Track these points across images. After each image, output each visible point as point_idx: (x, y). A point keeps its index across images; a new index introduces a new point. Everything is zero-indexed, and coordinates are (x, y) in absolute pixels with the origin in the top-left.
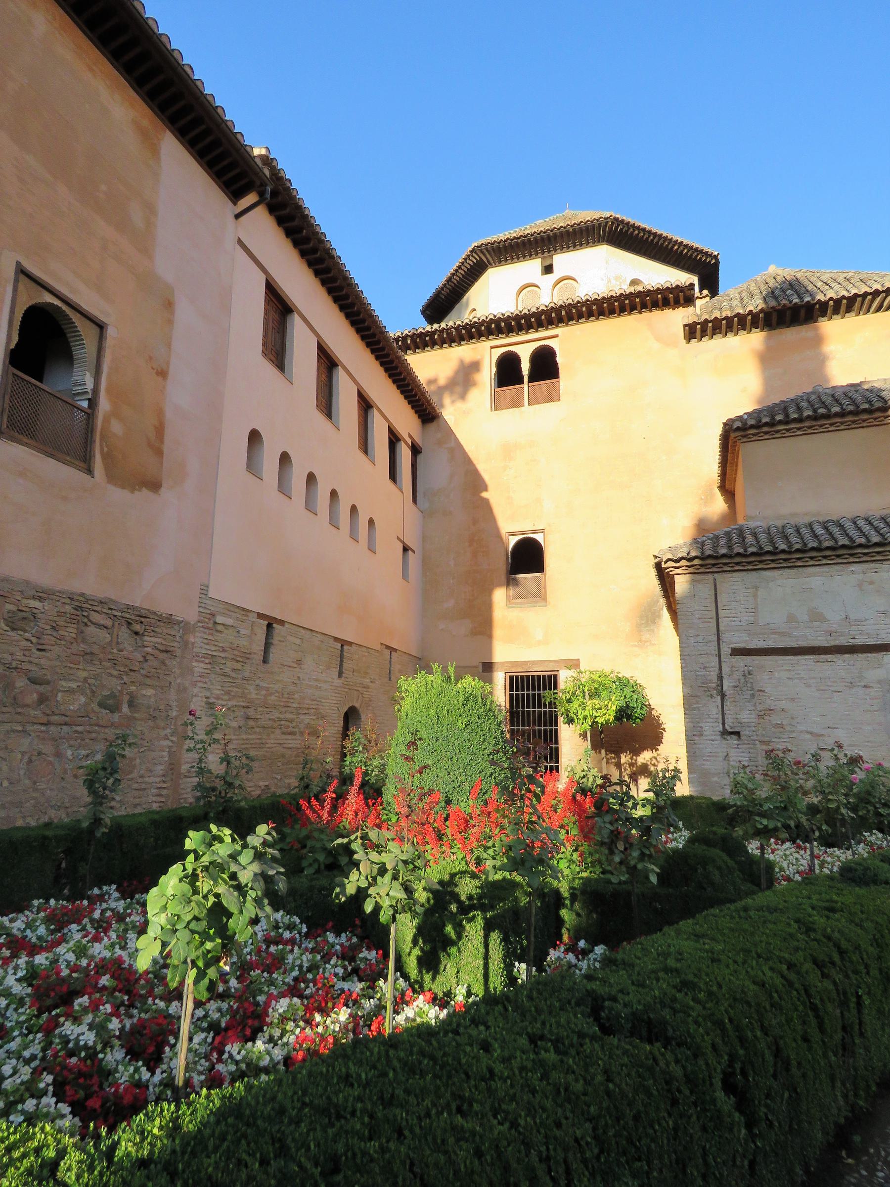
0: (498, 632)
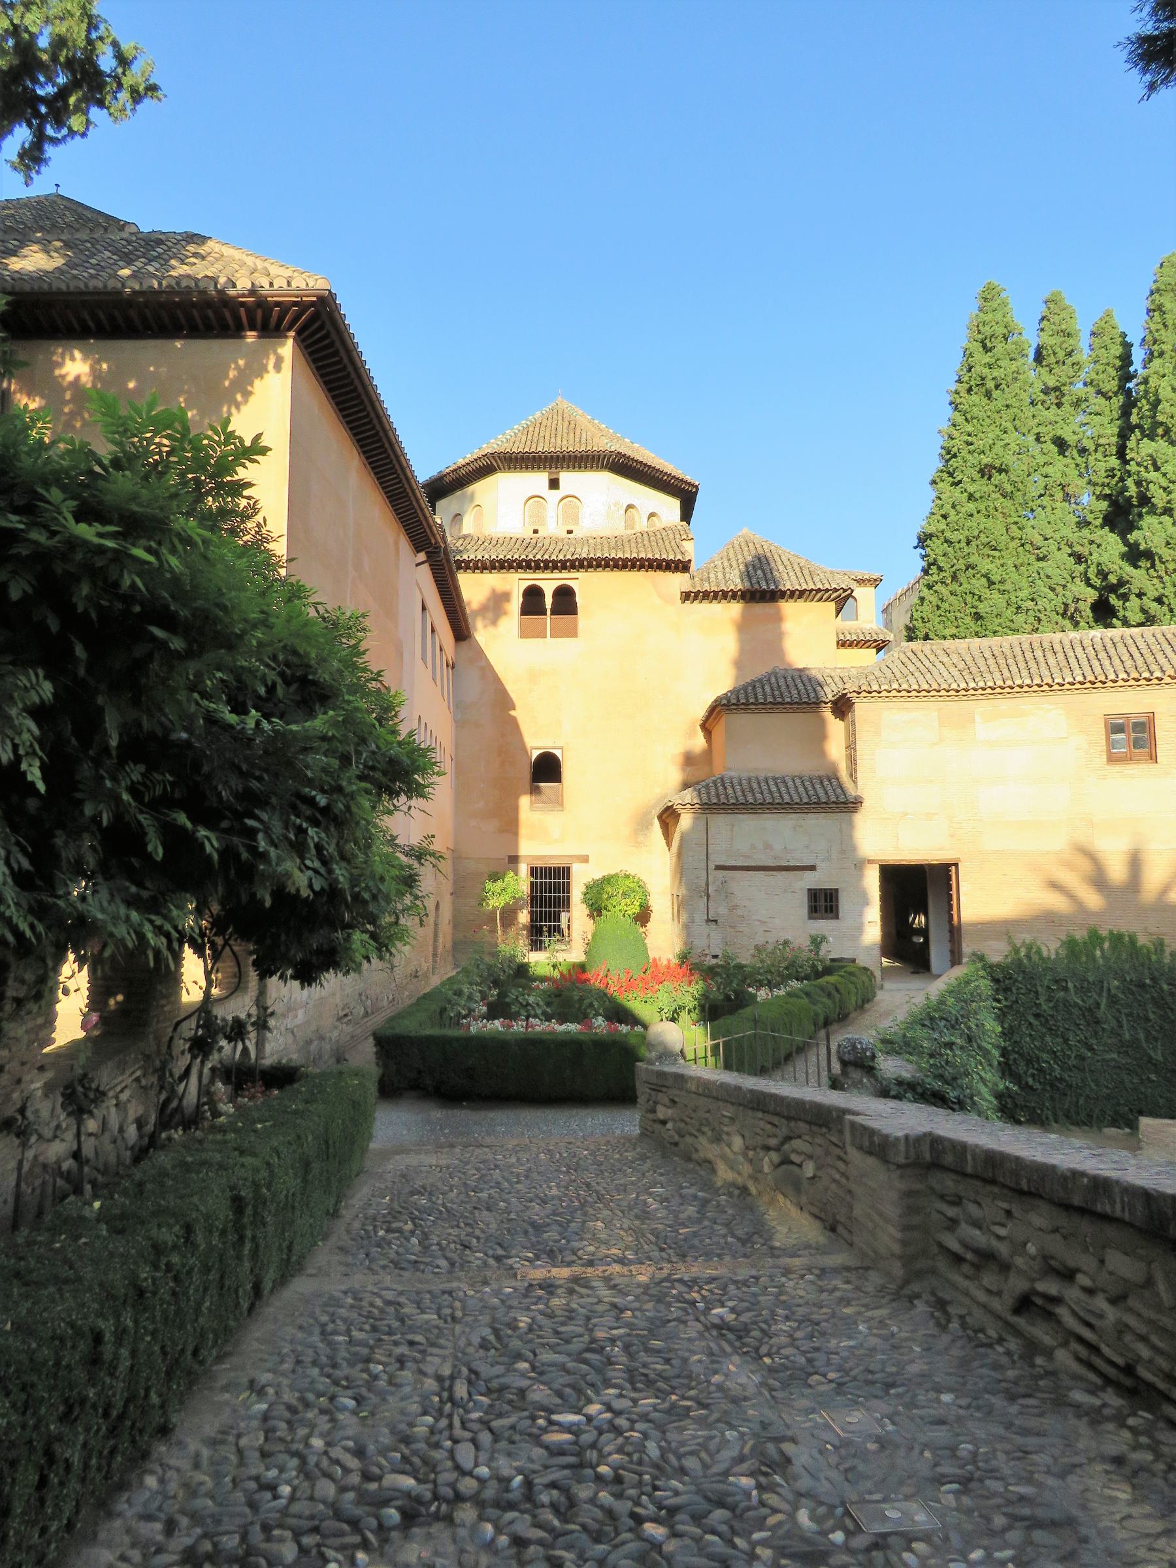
0: (523, 831)
